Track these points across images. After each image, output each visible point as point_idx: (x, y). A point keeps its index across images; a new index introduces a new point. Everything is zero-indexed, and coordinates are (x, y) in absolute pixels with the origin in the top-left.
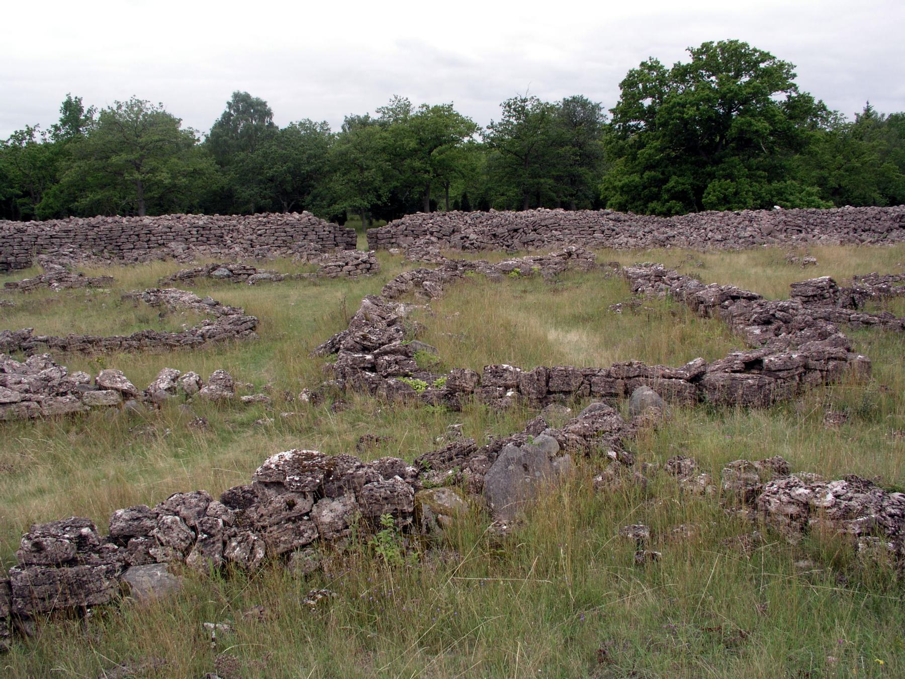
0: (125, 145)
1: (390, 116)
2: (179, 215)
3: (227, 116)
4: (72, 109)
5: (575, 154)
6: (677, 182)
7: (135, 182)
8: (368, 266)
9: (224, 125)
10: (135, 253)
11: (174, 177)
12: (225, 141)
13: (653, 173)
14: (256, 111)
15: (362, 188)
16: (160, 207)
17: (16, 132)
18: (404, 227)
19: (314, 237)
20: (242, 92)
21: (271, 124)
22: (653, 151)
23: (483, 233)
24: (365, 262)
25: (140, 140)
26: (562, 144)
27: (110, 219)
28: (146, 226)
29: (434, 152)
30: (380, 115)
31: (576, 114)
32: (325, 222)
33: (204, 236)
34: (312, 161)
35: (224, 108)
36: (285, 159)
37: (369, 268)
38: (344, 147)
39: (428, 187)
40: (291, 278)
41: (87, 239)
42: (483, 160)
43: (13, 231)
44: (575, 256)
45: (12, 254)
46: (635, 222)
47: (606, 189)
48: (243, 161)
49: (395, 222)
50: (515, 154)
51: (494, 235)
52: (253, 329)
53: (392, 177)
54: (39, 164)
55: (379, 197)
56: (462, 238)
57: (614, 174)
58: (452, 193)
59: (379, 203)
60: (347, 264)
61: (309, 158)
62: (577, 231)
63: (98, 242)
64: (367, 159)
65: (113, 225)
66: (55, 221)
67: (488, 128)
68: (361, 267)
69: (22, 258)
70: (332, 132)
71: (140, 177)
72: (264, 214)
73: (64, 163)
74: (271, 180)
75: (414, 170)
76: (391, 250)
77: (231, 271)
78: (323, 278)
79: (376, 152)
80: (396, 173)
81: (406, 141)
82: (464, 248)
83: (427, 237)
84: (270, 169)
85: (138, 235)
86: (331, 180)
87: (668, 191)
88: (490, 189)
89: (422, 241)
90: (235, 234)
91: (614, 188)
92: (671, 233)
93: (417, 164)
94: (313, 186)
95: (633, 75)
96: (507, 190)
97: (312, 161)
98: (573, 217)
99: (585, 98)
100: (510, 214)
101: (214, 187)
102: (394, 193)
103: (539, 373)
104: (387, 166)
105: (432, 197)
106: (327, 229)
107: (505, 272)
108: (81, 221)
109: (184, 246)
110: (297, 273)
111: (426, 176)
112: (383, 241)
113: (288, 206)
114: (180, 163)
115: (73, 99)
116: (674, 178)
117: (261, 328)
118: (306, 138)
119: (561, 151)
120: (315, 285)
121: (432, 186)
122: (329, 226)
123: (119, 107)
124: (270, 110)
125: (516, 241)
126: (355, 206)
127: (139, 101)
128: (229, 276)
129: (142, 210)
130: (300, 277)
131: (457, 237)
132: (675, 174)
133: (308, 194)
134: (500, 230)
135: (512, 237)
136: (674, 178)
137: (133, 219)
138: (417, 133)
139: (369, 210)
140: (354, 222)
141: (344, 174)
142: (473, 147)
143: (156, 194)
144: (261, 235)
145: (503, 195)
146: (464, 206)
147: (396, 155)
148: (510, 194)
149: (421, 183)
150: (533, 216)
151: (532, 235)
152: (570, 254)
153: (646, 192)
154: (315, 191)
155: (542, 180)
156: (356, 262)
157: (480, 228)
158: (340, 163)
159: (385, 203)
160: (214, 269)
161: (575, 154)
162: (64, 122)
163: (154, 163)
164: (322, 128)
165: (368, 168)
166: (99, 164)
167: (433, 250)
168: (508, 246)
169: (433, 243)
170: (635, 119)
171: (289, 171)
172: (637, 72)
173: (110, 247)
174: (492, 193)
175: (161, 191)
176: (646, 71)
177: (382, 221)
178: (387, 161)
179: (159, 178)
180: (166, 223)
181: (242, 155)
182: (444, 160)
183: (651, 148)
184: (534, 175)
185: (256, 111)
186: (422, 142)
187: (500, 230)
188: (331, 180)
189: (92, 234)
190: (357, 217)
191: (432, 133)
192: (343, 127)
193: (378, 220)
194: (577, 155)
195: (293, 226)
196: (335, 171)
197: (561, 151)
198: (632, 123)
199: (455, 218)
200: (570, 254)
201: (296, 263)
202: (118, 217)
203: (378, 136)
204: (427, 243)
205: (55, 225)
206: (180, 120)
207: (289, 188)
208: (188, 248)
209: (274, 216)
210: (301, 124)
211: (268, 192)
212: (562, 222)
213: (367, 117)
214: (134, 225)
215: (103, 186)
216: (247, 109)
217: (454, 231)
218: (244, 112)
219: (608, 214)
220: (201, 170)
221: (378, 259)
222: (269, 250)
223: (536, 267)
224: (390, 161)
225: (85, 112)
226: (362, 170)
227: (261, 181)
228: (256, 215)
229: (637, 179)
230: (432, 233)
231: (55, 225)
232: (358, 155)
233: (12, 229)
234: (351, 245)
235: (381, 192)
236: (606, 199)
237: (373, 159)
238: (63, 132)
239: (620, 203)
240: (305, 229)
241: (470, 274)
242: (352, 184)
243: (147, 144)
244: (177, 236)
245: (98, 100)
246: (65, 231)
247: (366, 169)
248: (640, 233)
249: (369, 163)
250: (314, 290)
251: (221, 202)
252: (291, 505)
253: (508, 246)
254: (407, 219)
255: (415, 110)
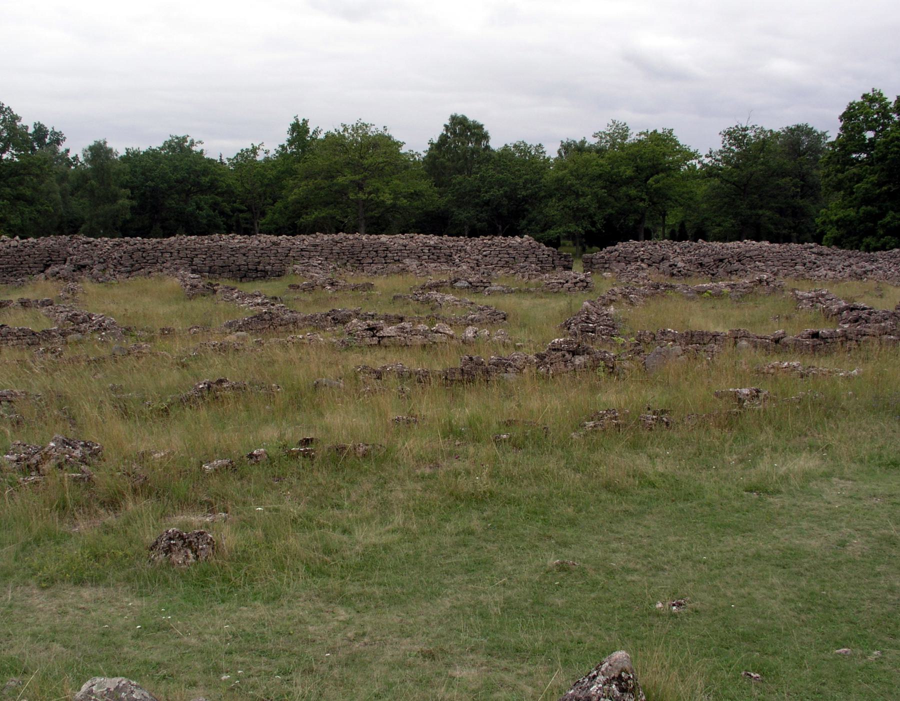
0: (355, 166)
1: (607, 141)
2: (412, 235)
3: (443, 139)
4: (299, 130)
5: (795, 185)
6: (894, 218)
7: (357, 202)
8: (585, 284)
9: (440, 147)
10: (374, 267)
11: (395, 198)
12: (442, 163)
13: (869, 208)
14: (473, 134)
15: (577, 214)
16: (378, 226)
17: (242, 150)
18: (617, 253)
19: (534, 259)
20: (459, 114)
21: (487, 147)
22: (869, 185)
23: (690, 261)
24: (582, 281)
25: (365, 162)
26: (784, 174)
27: (351, 236)
28: (383, 243)
29: (650, 181)
30: (597, 140)
31: (798, 141)
32: (543, 247)
33: (435, 255)
34: (529, 185)
35: (441, 130)
36: (501, 184)
37: (586, 286)
38: (560, 173)
39: (643, 215)
40: (520, 291)
41: (332, 253)
42: (701, 189)
43: (269, 244)
44: (765, 283)
45: (269, 264)
46: (839, 257)
47: (824, 223)
48: (460, 183)
49: (609, 248)
50: (734, 184)
51: (701, 264)
52: (505, 319)
53: (607, 204)
54: (266, 181)
55: (593, 224)
56: (670, 266)
57: (833, 209)
58: (671, 220)
59: (594, 229)
60: (567, 282)
61: (526, 182)
62: (780, 263)
63: (342, 256)
64: (583, 185)
65: (355, 241)
66: (304, 237)
67: (707, 156)
68: (578, 285)
69: (277, 267)
70: (547, 156)
71: (364, 198)
72: (488, 237)
73: (291, 182)
74: (487, 203)
75: (630, 199)
76: (605, 274)
77: (470, 283)
78: (546, 293)
79: (593, 179)
80: (611, 200)
81: (623, 168)
82: (673, 275)
83: (639, 263)
84: (486, 192)
85: (376, 252)
86: (546, 206)
87: (883, 226)
88: (707, 219)
89: (633, 266)
90: (462, 254)
91: (831, 222)
92: (869, 267)
93: (633, 192)
94: (527, 210)
95: (854, 108)
96: (723, 221)
97: (529, 185)
98: (778, 250)
99: (810, 126)
100: (717, 245)
101: (431, 208)
102: (608, 219)
103: (687, 333)
104: (603, 192)
105: (648, 224)
106: (546, 252)
107: (698, 292)
108: (326, 237)
109: (417, 262)
110: (524, 287)
111: (641, 204)
112: (597, 266)
113: (503, 229)
114: (403, 185)
115: (301, 122)
116: (891, 213)
117: (510, 319)
118: (521, 161)
119: (782, 181)
120: (541, 298)
121: (647, 214)
122: (549, 250)
123: (346, 129)
124: (487, 133)
125: (720, 270)
126: (569, 232)
127: (364, 124)
128: (468, 287)
129: (363, 229)
130: (528, 291)
131: (666, 264)
132: (892, 209)
133: (523, 219)
134: (706, 260)
135: (718, 267)
136: (891, 213)
137: (371, 237)
138: (634, 160)
139: (582, 236)
140: (568, 249)
141: (560, 200)
142: (693, 173)
143: (376, 213)
144: (486, 256)
145: (719, 225)
146: (678, 235)
147: (612, 182)
148: (727, 224)
149: (636, 211)
150: (739, 247)
151: (737, 265)
152: (760, 281)
153: (862, 227)
154: (531, 216)
155: (760, 212)
156: (574, 281)
157: (688, 257)
158: (556, 189)
159: (599, 230)
160: (455, 281)
161: (795, 185)
162: (291, 143)
163: (378, 185)
164: (537, 151)
165: (584, 195)
166: (325, 183)
167: (642, 274)
168: (713, 275)
169: (643, 269)
170: (855, 152)
171: (506, 195)
172: (858, 104)
173: (352, 261)
174: (708, 223)
175: (382, 210)
176: (867, 103)
177: (595, 248)
178: (602, 188)
179: (382, 198)
180: (401, 242)
181: (460, 178)
182: (660, 188)
183: (867, 183)
184: (752, 207)
185: (473, 134)
186: (638, 169)
187: (706, 260)
188: (546, 206)
189: (336, 249)
190: (570, 243)
191: (650, 160)
192: (559, 152)
193: (591, 246)
194: (797, 187)
195: (515, 249)
196: (551, 197)
197: (782, 181)
198: (854, 156)
199: (663, 247)
200: (760, 281)
201: (518, 281)
202: (357, 235)
203: (594, 163)
204: (637, 269)
205: (304, 240)
206: (404, 143)
207: (504, 211)
208: (421, 265)
209: (499, 239)
210: (515, 146)
211: (484, 215)
212: (766, 254)
213: (583, 142)
214: (373, 242)
215: (326, 204)
216: (463, 132)
217: (663, 259)
218: (461, 135)
219: (811, 248)
220: (420, 191)
221: (593, 280)
222: (493, 269)
223: (726, 290)
224: (605, 188)
225: (311, 133)
226: (578, 196)
227: (477, 204)
228: (482, 237)
229: (853, 214)
230: (642, 260)
231: (304, 240)
232: (575, 182)
233: (268, 242)
234: (569, 268)
235: (596, 218)
236: (823, 233)
237: (588, 186)
238: (289, 151)
239: (835, 238)
240: (526, 252)
241: (670, 293)
242: (567, 210)
243: (370, 166)
244: (411, 253)
245: (325, 123)
246: (314, 246)
247: (582, 196)
248: (840, 267)
249: (586, 189)
250: (538, 301)
251: (436, 223)
252: (564, 356)
253: (713, 275)
254: (620, 246)
255: (633, 137)
